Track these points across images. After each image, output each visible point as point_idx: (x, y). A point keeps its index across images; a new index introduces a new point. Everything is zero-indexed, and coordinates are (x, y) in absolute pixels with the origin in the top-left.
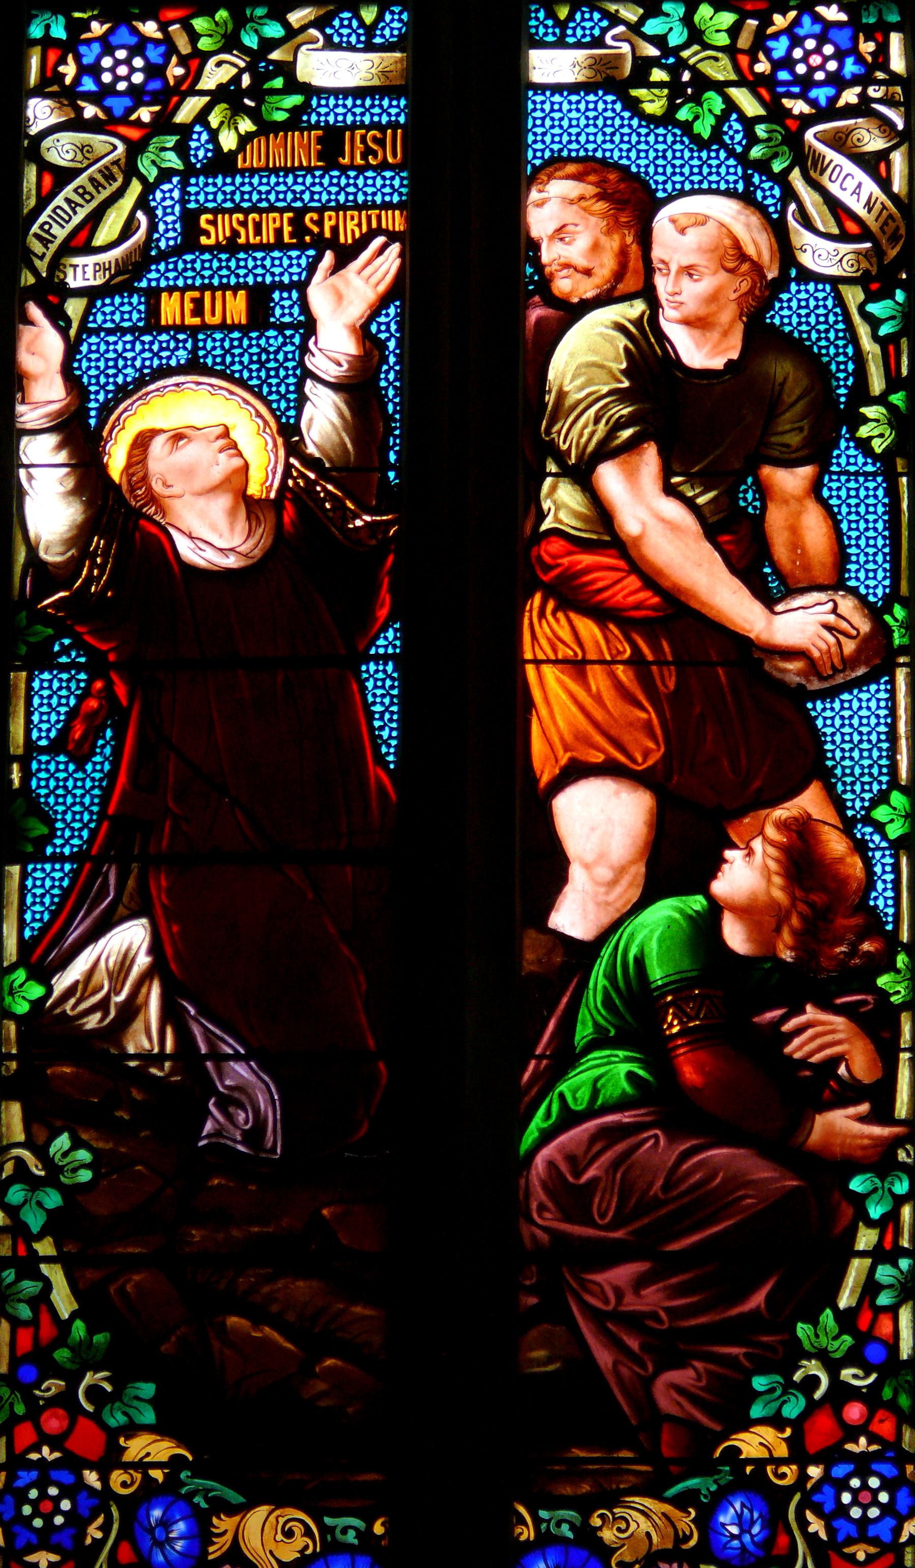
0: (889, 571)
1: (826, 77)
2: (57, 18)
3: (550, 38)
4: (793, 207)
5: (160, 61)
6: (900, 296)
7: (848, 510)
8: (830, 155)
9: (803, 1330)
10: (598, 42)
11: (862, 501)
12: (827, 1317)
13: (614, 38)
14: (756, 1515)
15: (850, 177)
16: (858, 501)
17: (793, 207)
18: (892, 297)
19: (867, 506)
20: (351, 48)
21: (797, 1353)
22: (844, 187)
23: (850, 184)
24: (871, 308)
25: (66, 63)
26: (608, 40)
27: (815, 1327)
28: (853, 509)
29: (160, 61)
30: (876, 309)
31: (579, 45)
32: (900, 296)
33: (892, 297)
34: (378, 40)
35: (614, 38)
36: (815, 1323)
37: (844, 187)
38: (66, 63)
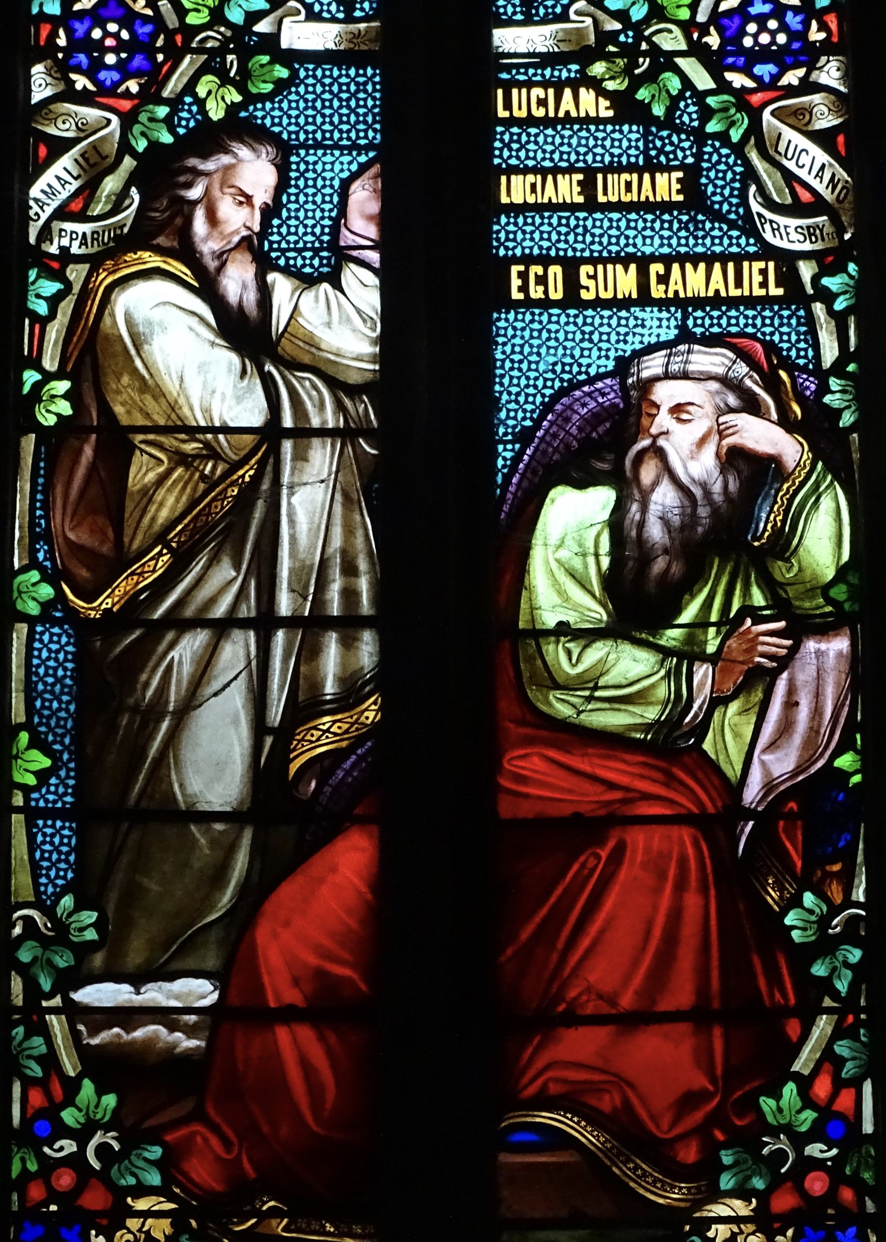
0: (495, 383)
1: (117, 61)
2: (79, 1123)
3: (519, 17)
4: (753, 189)
5: (799, 27)
6: (852, 267)
7: (511, 365)
8: (789, 134)
9: (767, 1104)
10: (564, 17)
11: (526, 357)
12: (790, 1090)
13: (577, 13)
14: (295, 743)
15: (804, 153)
16: (522, 357)
17: (753, 189)
18: (845, 270)
19: (530, 363)
20: (334, 20)
21: (763, 1127)
22: (800, 164)
23: (805, 159)
24: (826, 281)
25: (709, 34)
26: (573, 17)
27: (778, 1101)
28: (516, 365)
29: (799, 27)
30: (832, 283)
31: (544, 21)
32: (852, 267)
33: (845, 270)
34: (358, 14)
35: (577, 13)
36: (778, 1097)
37: (800, 164)
38: (709, 34)
